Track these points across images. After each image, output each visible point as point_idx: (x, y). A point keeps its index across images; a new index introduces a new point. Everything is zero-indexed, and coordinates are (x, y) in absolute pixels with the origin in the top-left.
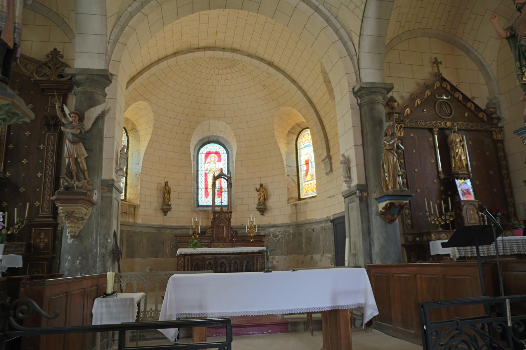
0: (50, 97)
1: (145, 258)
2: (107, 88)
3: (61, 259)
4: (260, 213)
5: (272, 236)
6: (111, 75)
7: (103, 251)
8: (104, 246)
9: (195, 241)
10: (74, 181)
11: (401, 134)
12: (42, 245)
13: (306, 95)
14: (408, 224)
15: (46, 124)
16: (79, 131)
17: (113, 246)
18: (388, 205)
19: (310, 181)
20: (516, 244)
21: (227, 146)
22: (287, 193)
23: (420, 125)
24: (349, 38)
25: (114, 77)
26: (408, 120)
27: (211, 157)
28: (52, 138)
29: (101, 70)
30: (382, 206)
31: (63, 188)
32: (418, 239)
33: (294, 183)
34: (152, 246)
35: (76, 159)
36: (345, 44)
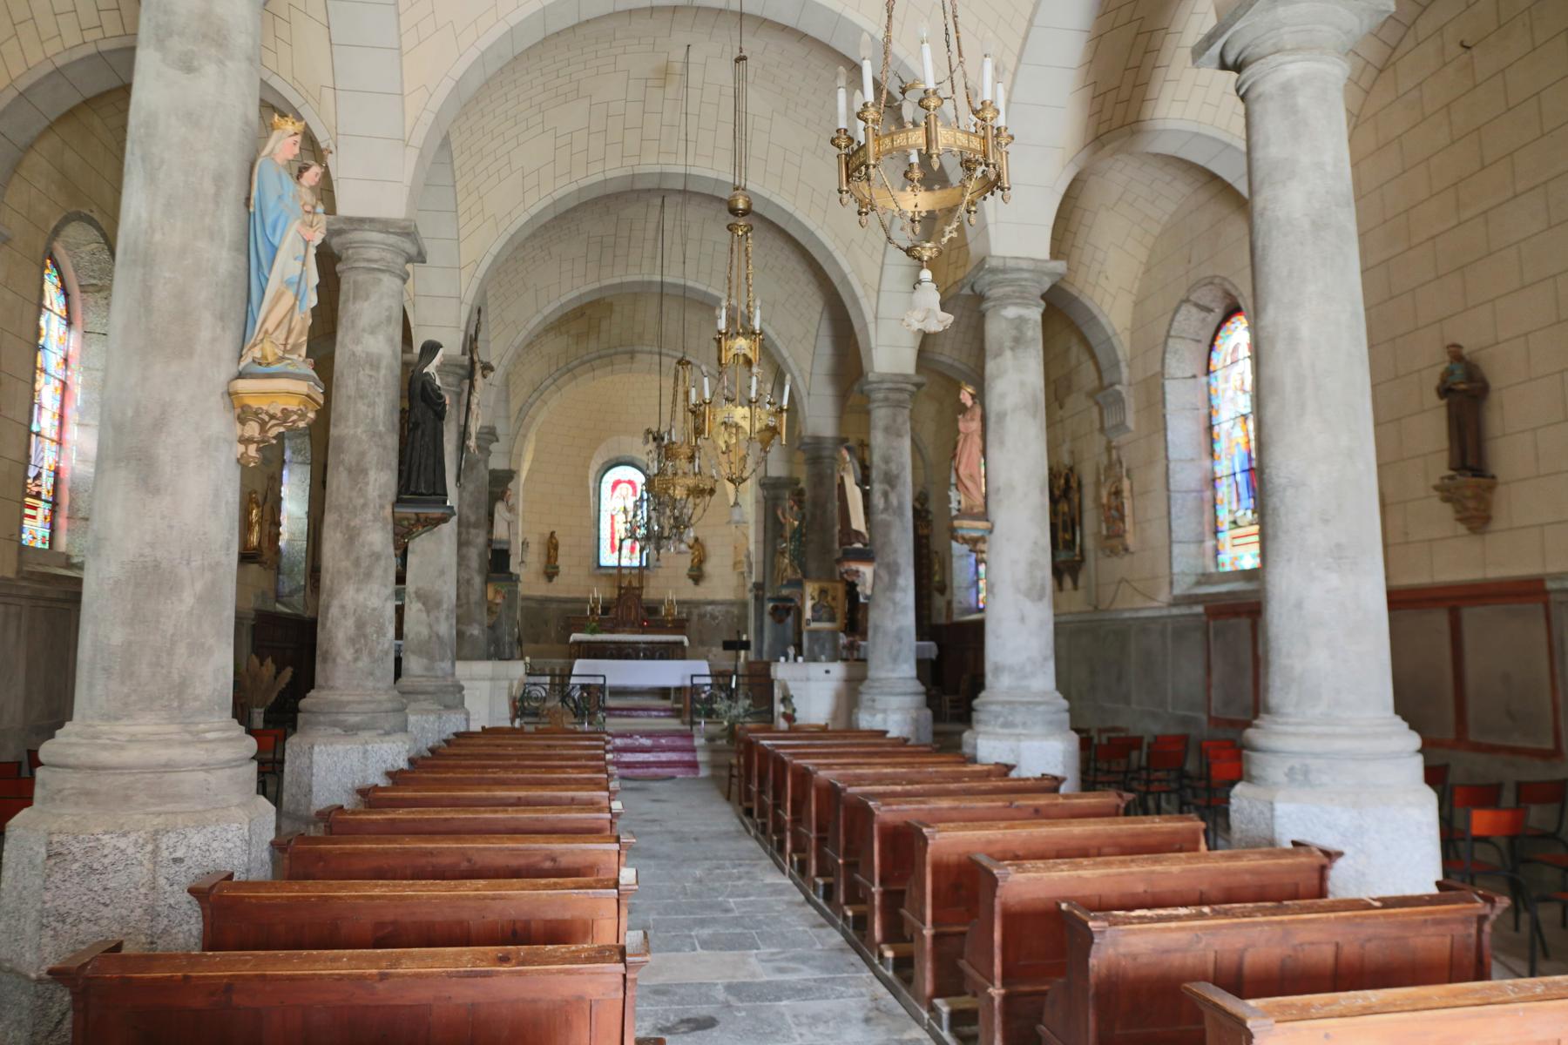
9: (594, 624)
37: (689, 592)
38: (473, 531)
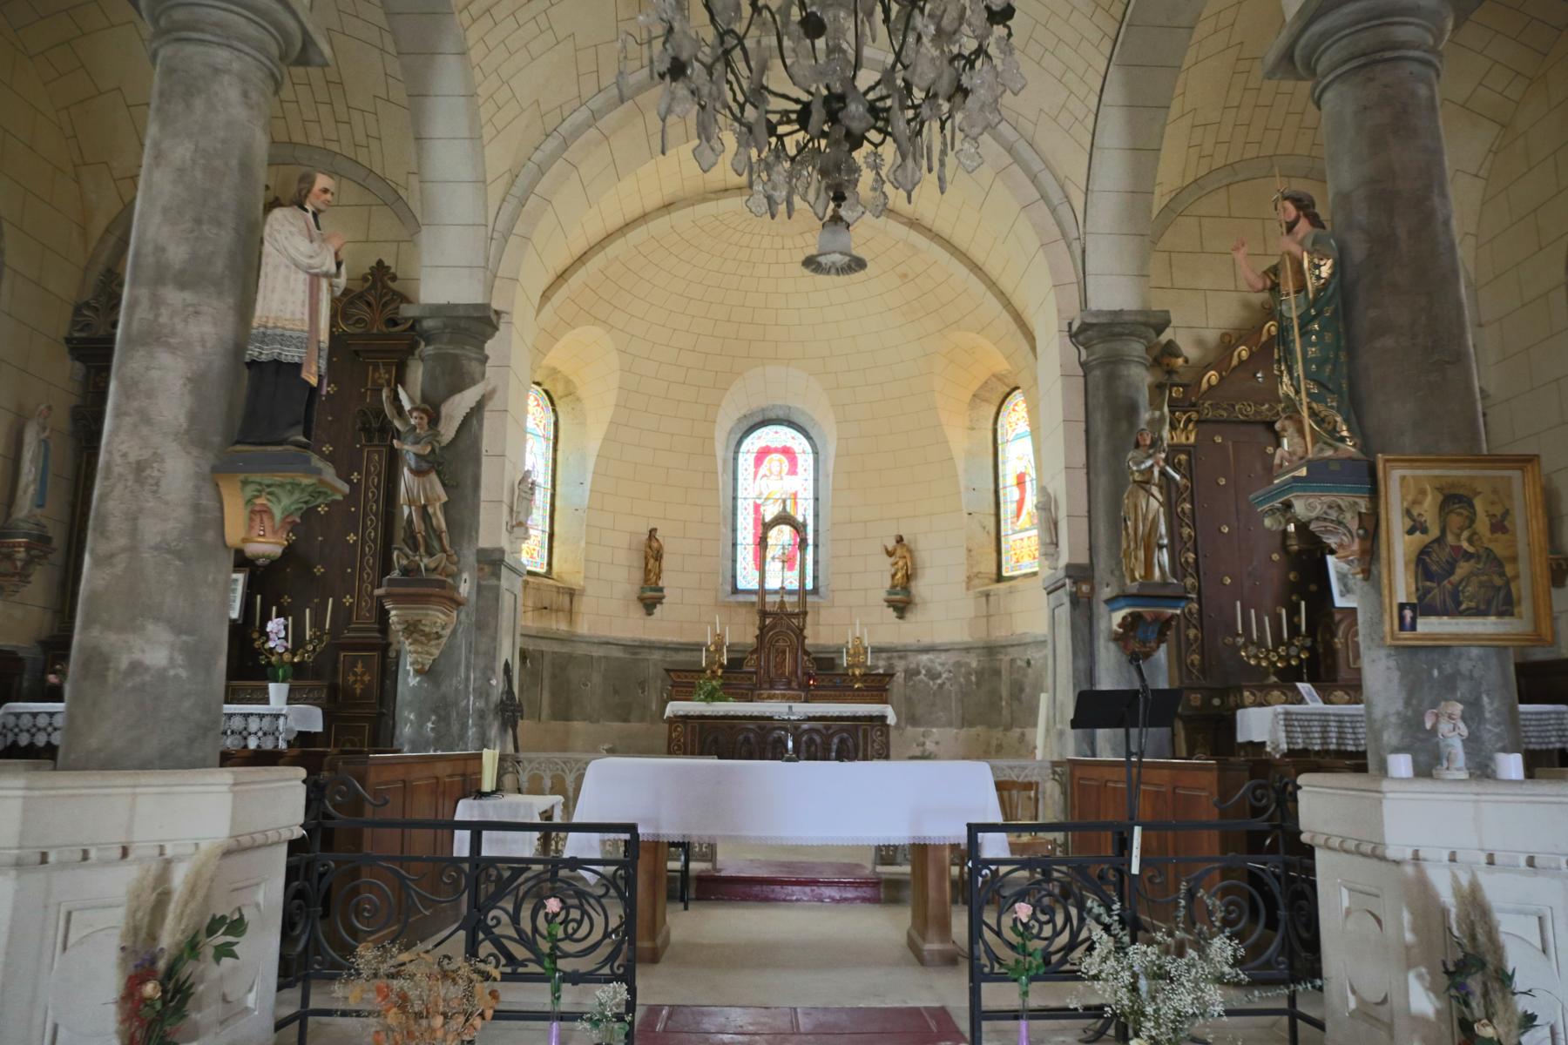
0: (371, 368)
1: (598, 721)
2: (489, 342)
3: (396, 718)
4: (895, 614)
5: (925, 675)
6: (497, 313)
7: (480, 704)
8: (483, 693)
10: (421, 556)
11: (1187, 438)
12: (358, 688)
13: (1010, 303)
14: (1192, 664)
15: (363, 429)
16: (429, 449)
17: (502, 693)
18: (1129, 619)
19: (1027, 530)
20: (1321, 723)
21: (812, 434)
22: (965, 562)
23: (1242, 414)
24: (1061, 195)
25: (504, 318)
26: (1209, 402)
27: (772, 459)
28: (376, 458)
29: (475, 306)
30: (1118, 617)
31: (397, 571)
32: (1216, 702)
33: (986, 534)
34: (616, 692)
35: (424, 508)
36: (1053, 211)
37: (883, 630)
38: (174, 297)
